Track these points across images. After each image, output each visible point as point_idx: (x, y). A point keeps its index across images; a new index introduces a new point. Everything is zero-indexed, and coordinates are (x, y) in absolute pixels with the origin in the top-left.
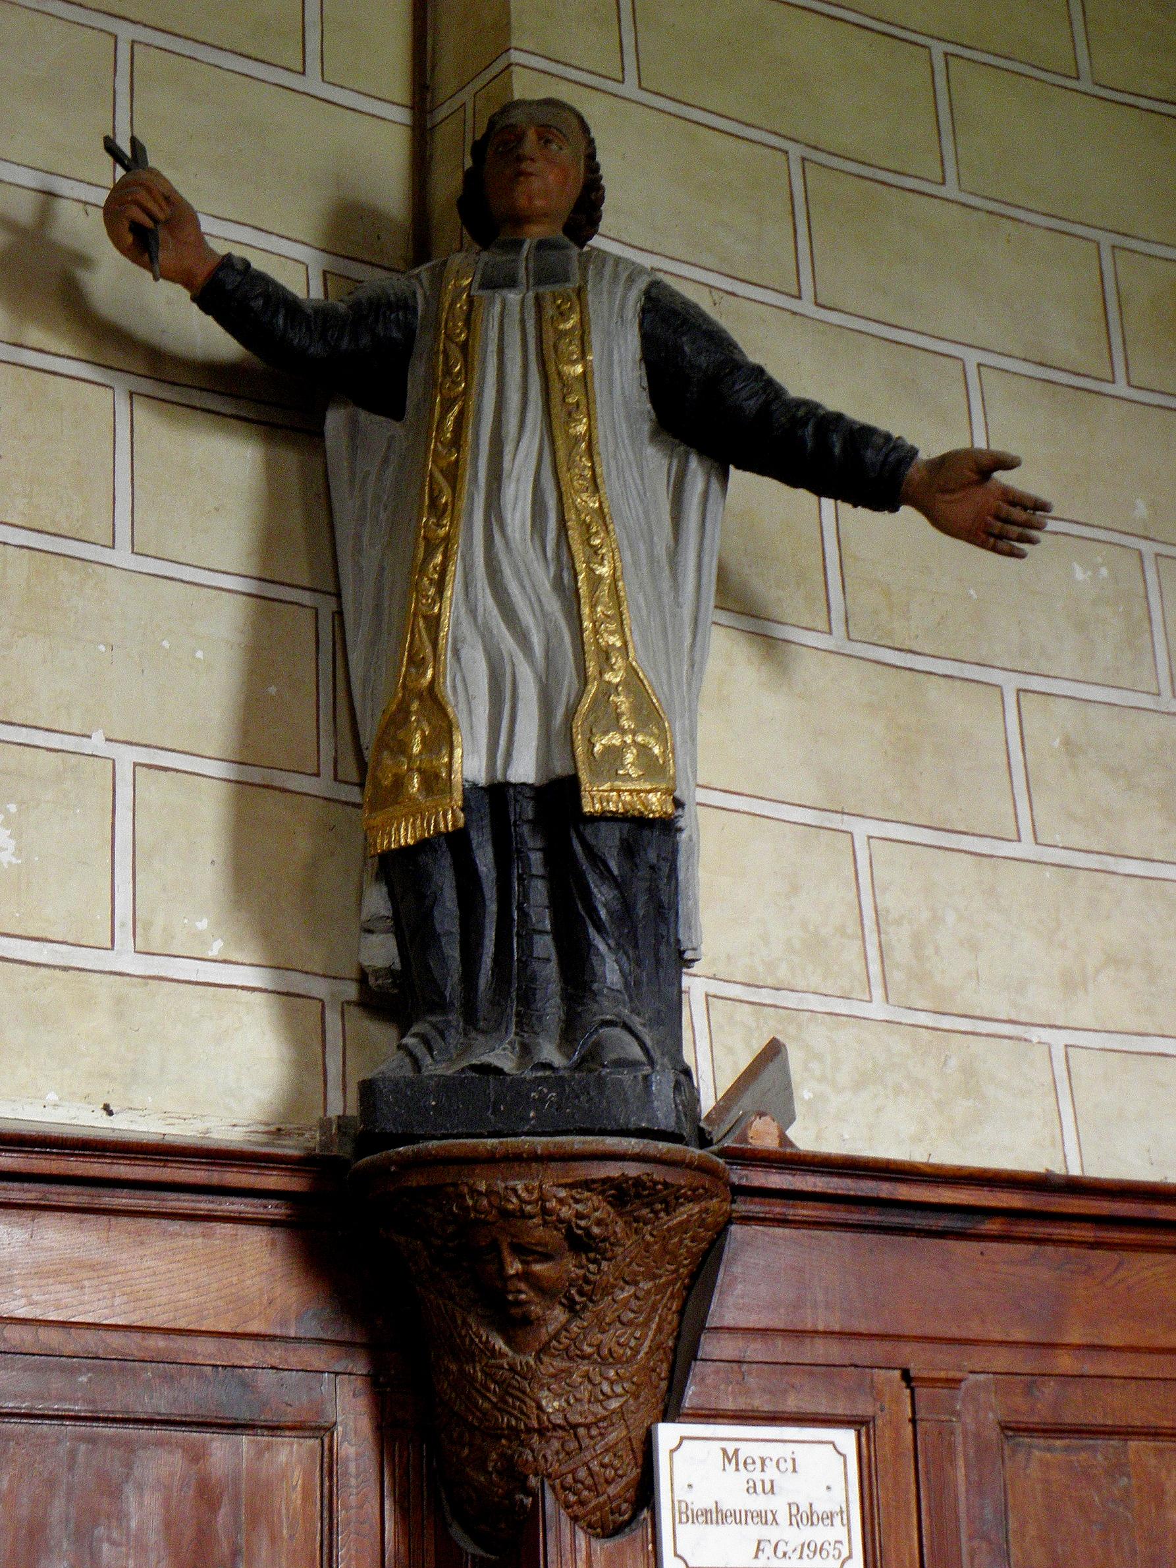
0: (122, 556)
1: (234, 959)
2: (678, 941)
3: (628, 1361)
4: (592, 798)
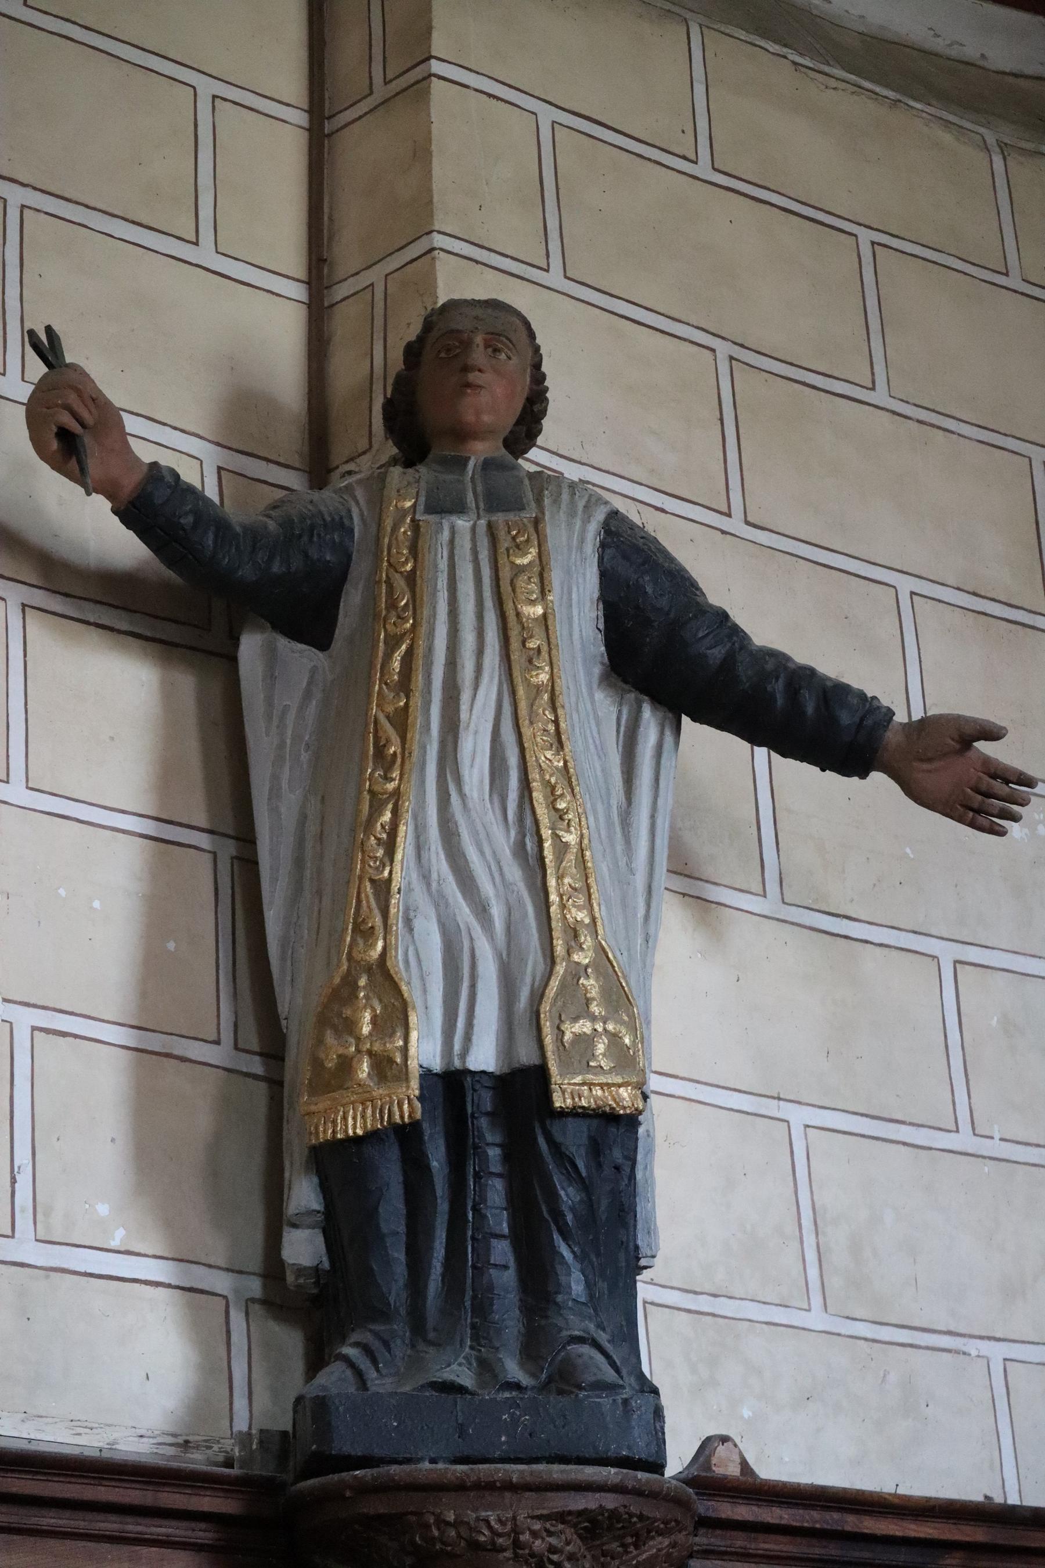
0: (16, 792)
1: (137, 1250)
4: (563, 1092)
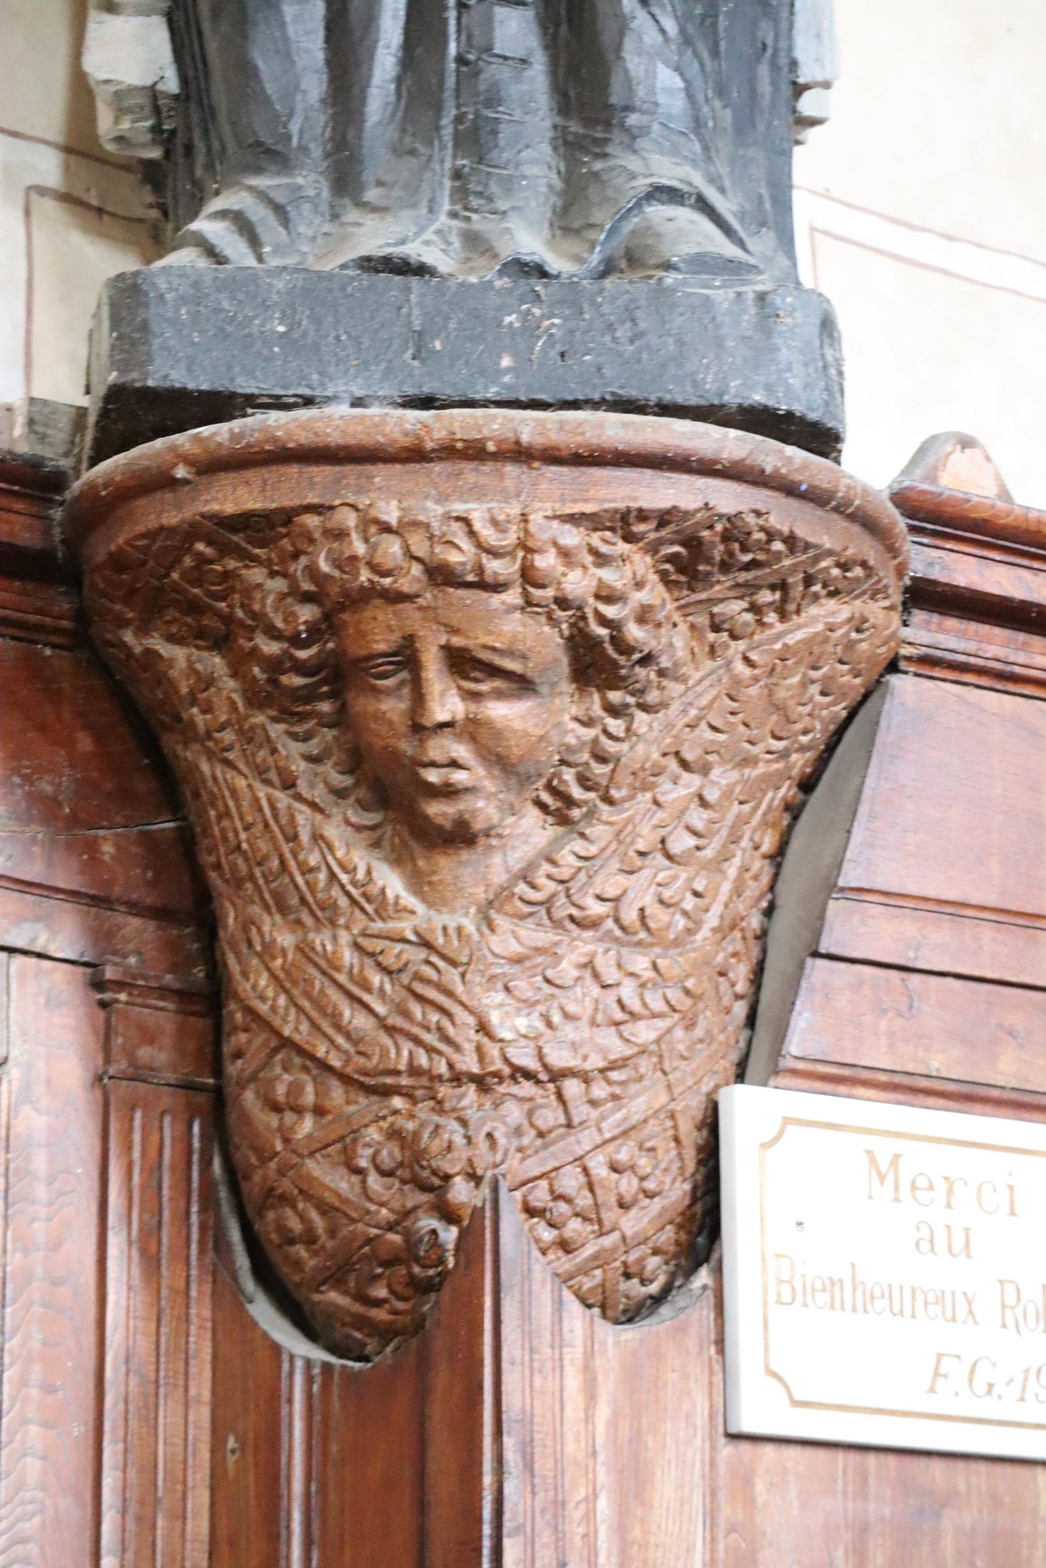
2: (794, 64)
3: (676, 943)
